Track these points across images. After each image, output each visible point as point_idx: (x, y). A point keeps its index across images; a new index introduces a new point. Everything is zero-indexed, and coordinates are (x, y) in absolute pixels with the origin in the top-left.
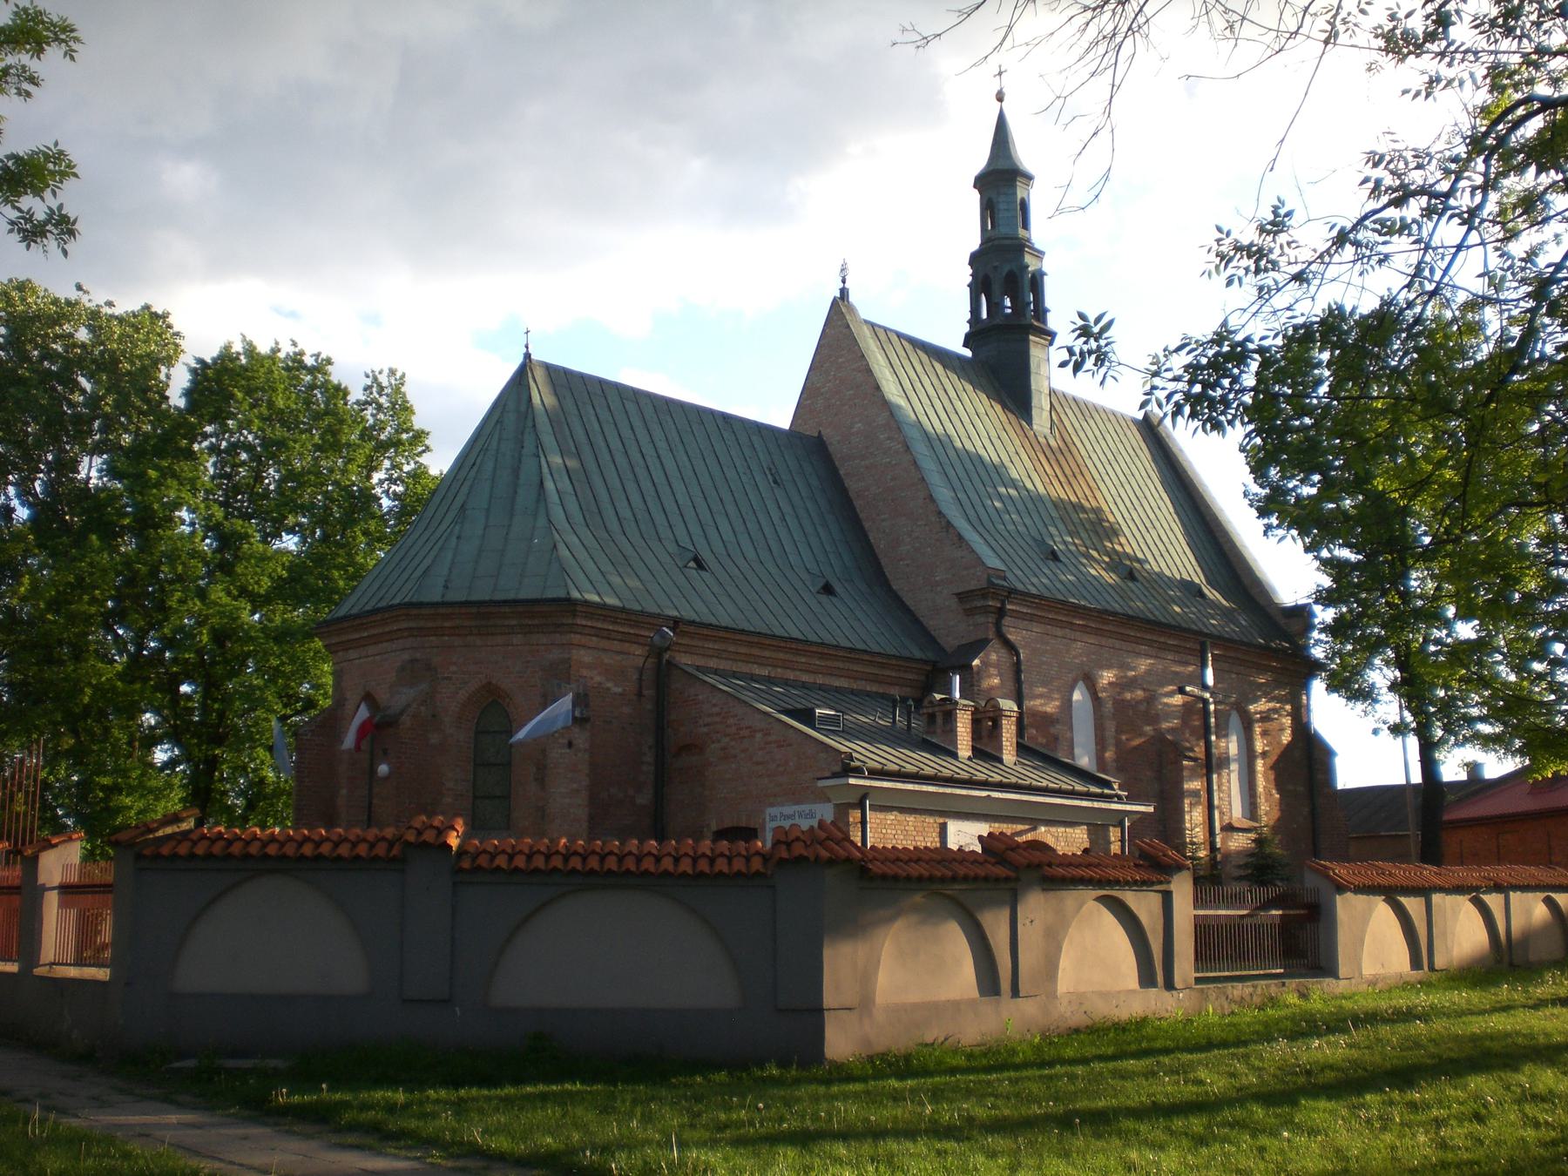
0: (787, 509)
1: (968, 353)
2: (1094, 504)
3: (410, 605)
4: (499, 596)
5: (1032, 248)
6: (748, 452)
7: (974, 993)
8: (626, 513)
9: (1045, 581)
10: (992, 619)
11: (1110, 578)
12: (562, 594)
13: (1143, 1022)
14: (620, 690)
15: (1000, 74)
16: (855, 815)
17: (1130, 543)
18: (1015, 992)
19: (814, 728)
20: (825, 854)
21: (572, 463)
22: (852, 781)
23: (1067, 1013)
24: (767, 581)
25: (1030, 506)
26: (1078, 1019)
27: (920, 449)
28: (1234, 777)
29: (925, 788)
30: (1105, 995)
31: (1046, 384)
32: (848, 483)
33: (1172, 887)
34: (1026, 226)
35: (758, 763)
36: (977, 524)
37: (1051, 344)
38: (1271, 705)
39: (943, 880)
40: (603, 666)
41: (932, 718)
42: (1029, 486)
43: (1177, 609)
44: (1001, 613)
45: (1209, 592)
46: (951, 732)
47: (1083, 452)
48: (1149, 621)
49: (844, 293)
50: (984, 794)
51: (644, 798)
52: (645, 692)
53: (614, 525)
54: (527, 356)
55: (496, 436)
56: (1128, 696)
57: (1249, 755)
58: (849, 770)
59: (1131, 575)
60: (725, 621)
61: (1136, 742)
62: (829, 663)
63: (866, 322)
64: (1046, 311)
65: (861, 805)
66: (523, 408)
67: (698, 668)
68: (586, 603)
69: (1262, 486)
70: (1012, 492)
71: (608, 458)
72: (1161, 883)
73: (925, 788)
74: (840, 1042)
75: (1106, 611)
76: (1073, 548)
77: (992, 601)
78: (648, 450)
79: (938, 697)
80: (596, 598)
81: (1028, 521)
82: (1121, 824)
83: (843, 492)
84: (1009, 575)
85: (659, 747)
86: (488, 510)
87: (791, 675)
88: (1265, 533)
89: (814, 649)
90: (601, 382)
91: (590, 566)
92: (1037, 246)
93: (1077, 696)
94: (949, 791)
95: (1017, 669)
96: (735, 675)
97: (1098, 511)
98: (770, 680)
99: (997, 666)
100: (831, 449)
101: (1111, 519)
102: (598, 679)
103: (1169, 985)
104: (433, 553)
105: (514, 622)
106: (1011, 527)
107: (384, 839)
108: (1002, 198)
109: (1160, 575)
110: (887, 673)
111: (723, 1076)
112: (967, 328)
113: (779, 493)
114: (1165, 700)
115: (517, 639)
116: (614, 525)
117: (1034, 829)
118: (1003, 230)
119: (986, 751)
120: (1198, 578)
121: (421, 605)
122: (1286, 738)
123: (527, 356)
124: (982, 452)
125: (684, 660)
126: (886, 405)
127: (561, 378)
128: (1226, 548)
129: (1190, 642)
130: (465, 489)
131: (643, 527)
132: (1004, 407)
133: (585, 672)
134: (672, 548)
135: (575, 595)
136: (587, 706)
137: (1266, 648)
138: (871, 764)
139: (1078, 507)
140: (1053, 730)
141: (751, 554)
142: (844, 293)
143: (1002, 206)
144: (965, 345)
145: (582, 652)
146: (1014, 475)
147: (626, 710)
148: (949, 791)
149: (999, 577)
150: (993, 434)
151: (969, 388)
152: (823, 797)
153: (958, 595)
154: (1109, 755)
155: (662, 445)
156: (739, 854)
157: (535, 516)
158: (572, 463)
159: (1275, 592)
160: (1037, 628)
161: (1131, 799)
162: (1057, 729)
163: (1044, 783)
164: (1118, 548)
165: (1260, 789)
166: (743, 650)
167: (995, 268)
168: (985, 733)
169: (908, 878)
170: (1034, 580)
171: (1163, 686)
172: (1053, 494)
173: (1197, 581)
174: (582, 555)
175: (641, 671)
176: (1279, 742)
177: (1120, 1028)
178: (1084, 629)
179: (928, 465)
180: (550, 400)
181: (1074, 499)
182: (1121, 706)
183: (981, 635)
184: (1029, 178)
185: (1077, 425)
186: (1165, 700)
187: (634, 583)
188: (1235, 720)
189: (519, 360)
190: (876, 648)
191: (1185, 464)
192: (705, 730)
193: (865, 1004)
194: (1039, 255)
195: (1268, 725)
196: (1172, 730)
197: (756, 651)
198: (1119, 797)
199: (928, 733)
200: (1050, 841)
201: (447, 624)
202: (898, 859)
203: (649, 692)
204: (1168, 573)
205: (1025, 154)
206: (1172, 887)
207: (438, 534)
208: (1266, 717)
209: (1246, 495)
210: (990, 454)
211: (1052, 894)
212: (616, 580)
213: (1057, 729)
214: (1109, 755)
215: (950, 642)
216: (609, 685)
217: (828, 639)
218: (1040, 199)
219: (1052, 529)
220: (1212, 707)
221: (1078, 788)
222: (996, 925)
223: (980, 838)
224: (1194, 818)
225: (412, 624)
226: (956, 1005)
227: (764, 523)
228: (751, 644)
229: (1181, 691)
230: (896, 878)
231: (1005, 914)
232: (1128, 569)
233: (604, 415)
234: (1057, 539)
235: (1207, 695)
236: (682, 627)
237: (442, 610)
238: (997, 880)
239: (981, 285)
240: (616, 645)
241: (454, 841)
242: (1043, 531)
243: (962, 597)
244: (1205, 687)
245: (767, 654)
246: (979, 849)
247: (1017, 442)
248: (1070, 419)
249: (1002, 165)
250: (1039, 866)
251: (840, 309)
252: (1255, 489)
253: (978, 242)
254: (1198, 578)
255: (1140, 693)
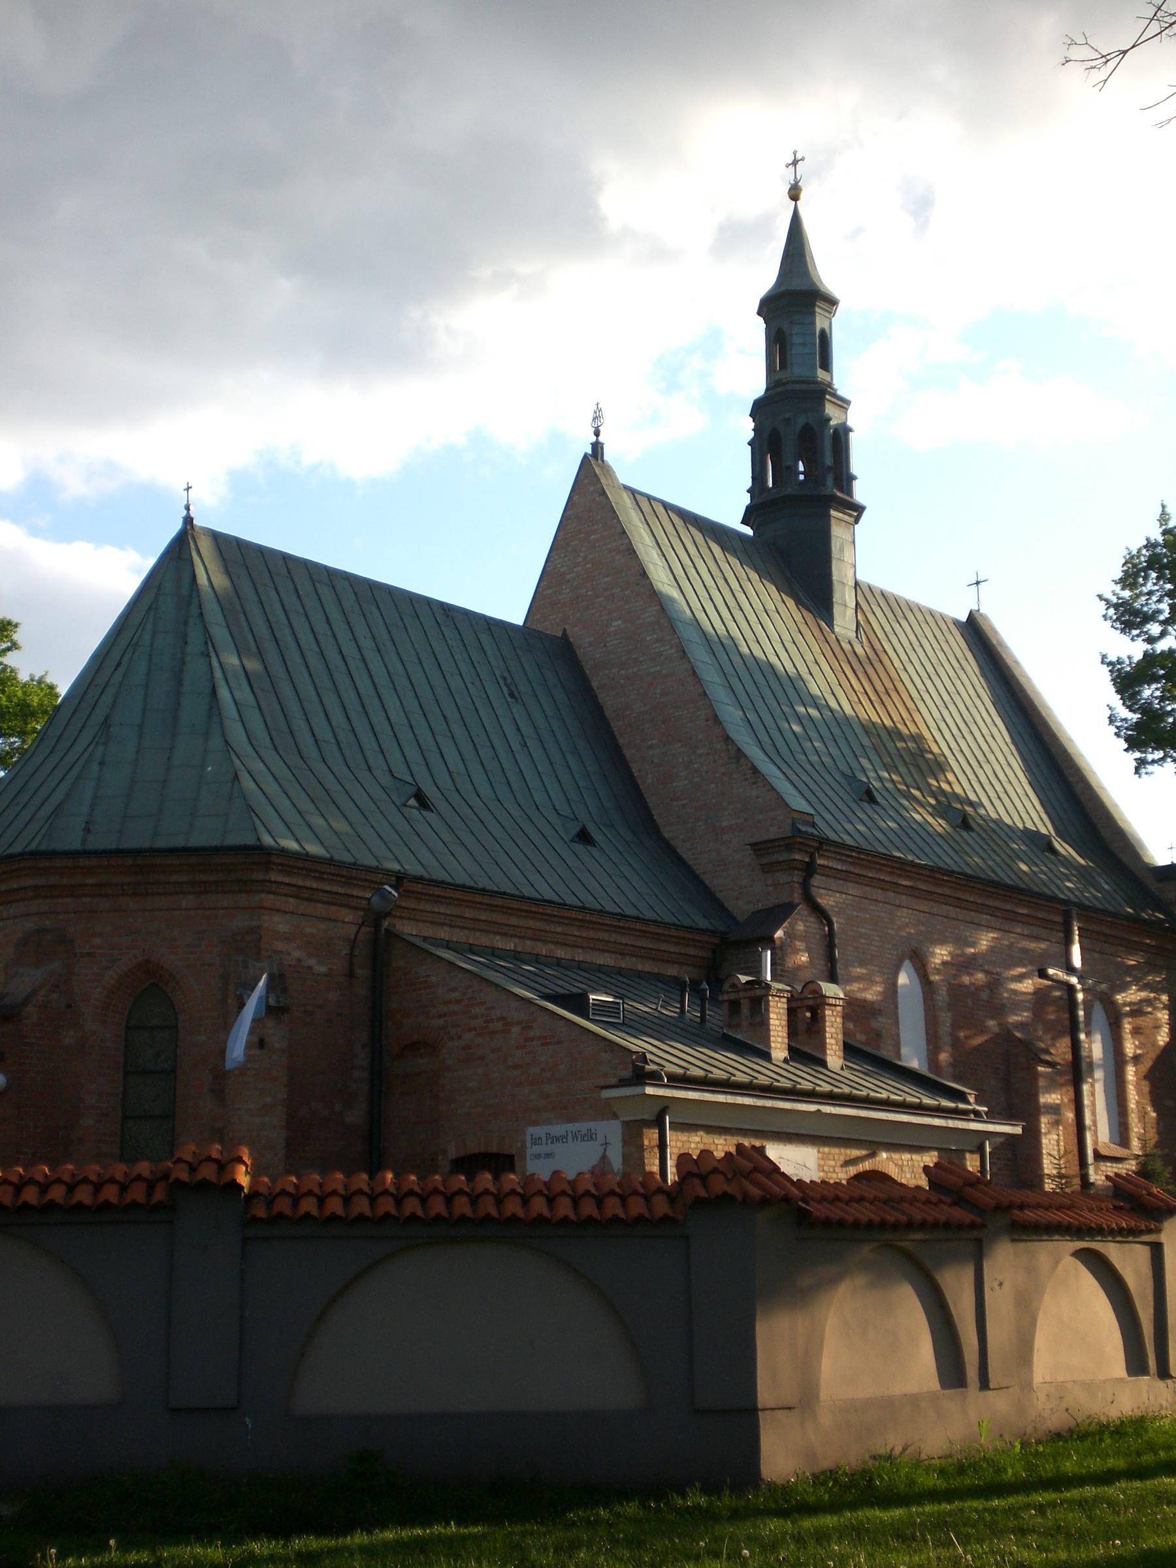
0: (527, 730)
1: (748, 531)
2: (913, 729)
3: (37, 854)
4: (161, 843)
5: (834, 395)
6: (476, 656)
7: (934, 1384)
8: (324, 733)
9: (861, 828)
10: (797, 877)
11: (939, 825)
12: (250, 840)
13: (1139, 1424)
14: (323, 969)
15: (795, 163)
16: (651, 1136)
17: (960, 782)
18: (984, 1384)
19: (588, 1019)
20: (755, 1191)
21: (253, 665)
22: (650, 1090)
23: (1047, 1412)
24: (509, 826)
25: (836, 731)
26: (1055, 1420)
27: (699, 655)
28: (1099, 1088)
29: (740, 1100)
30: (1089, 1387)
31: (850, 573)
32: (602, 697)
33: (1163, 1238)
34: (826, 364)
35: (516, 1067)
36: (774, 754)
37: (857, 521)
38: (1143, 994)
39: (896, 1227)
40: (303, 937)
41: (735, 1006)
42: (833, 704)
43: (1024, 867)
44: (810, 869)
45: (1058, 844)
46: (763, 1025)
47: (897, 664)
48: (992, 883)
49: (597, 448)
50: (812, 1108)
51: (356, 1116)
52: (359, 972)
53: (310, 750)
54: (188, 520)
55: (149, 627)
56: (966, 980)
57: (1117, 1061)
58: (641, 1075)
59: (965, 823)
60: (461, 878)
61: (978, 1040)
62: (592, 934)
63: (626, 488)
64: (852, 478)
65: (659, 1123)
66: (185, 592)
67: (425, 939)
68: (284, 851)
69: (1131, 709)
70: (813, 712)
71: (299, 660)
72: (1150, 1231)
73: (740, 1100)
74: (781, 1456)
75: (939, 870)
76: (889, 785)
77: (797, 854)
78: (349, 650)
79: (744, 979)
80: (293, 845)
81: (834, 750)
82: (980, 1150)
83: (598, 710)
84: (817, 820)
85: (377, 1052)
86: (141, 727)
87: (543, 949)
88: (1137, 771)
89: (573, 914)
90: (286, 558)
91: (284, 803)
92: (841, 392)
93: (903, 979)
94: (769, 1103)
95: (830, 946)
96: (472, 949)
97: (918, 739)
98: (516, 956)
99: (803, 938)
100: (580, 653)
101: (935, 750)
102: (297, 954)
103: (1164, 1373)
104: (65, 785)
105: (183, 878)
106: (814, 758)
107: (139, 1178)
108: (796, 329)
109: (999, 822)
110: (664, 947)
111: (631, 1508)
112: (746, 500)
113: (517, 709)
114: (1013, 986)
115: (186, 902)
116: (310, 750)
117: (873, 1155)
118: (797, 371)
119: (806, 1051)
120: (1045, 828)
121: (53, 854)
122: (1163, 1038)
123: (188, 520)
124: (774, 660)
125: (408, 929)
126: (654, 596)
127: (233, 551)
128: (1078, 789)
129: (1050, 914)
130: (108, 697)
131: (347, 753)
132: (799, 602)
133: (279, 945)
134: (386, 781)
135: (267, 840)
136: (284, 990)
137: (1135, 920)
138: (670, 1068)
139: (894, 734)
140: (874, 1024)
141: (486, 791)
142: (597, 448)
143: (797, 340)
144: (743, 522)
145: (277, 918)
146: (815, 690)
147: (333, 996)
148: (769, 1103)
149: (806, 823)
150: (786, 637)
151: (754, 576)
152: (607, 1111)
153: (754, 845)
154: (944, 1057)
155: (367, 644)
156: (636, 1193)
157: (207, 736)
158: (253, 665)
159: (1143, 847)
160: (853, 889)
161: (992, 1116)
162: (879, 1023)
163: (884, 1095)
164: (945, 786)
165: (1132, 1105)
166: (483, 916)
167: (787, 420)
168: (802, 1027)
169: (856, 1225)
170: (848, 827)
171: (1010, 967)
172: (863, 716)
173: (1043, 831)
174: (272, 788)
175: (353, 943)
176: (1154, 1044)
177: (1120, 1430)
178: (912, 892)
179: (710, 675)
180: (221, 581)
181: (888, 723)
182: (958, 992)
183: (784, 899)
184: (832, 302)
185: (887, 628)
186: (1013, 986)
187: (341, 826)
188: (1099, 1013)
189: (178, 526)
190: (650, 915)
191: (1022, 680)
192: (441, 1022)
193: (805, 1401)
194: (843, 404)
195: (1140, 1021)
196: (1021, 1026)
197: (499, 918)
198: (977, 1113)
199: (730, 1026)
200: (893, 1171)
201: (89, 881)
202: (838, 1198)
203: (361, 972)
204: (1008, 821)
205: (828, 271)
206: (1163, 1238)
207: (71, 758)
208: (1137, 1011)
209: (1111, 720)
210: (784, 663)
211: (1022, 1245)
212: (318, 821)
213: (879, 1023)
214: (944, 1057)
215: (742, 908)
216: (312, 962)
217: (590, 902)
218: (843, 329)
219: (864, 762)
220: (1080, 996)
221: (927, 1101)
222: (957, 1286)
223: (926, 1169)
224: (1052, 1145)
225: (42, 881)
226: (914, 1400)
227: (500, 750)
228: (493, 908)
229: (1043, 974)
230: (841, 1224)
231: (968, 1273)
232: (961, 816)
233: (291, 601)
234: (872, 774)
235: (1074, 980)
236: (406, 883)
237: (84, 862)
238: (960, 1227)
239: (766, 444)
240: (320, 910)
241: (244, 1180)
242: (854, 764)
243: (759, 848)
244: (1070, 970)
245: (514, 921)
246: (924, 1182)
247: (816, 649)
248: (879, 620)
249: (796, 285)
250: (1010, 1207)
251: (592, 470)
252: (1124, 713)
253: (764, 387)
254: (1045, 828)
255: (980, 976)
